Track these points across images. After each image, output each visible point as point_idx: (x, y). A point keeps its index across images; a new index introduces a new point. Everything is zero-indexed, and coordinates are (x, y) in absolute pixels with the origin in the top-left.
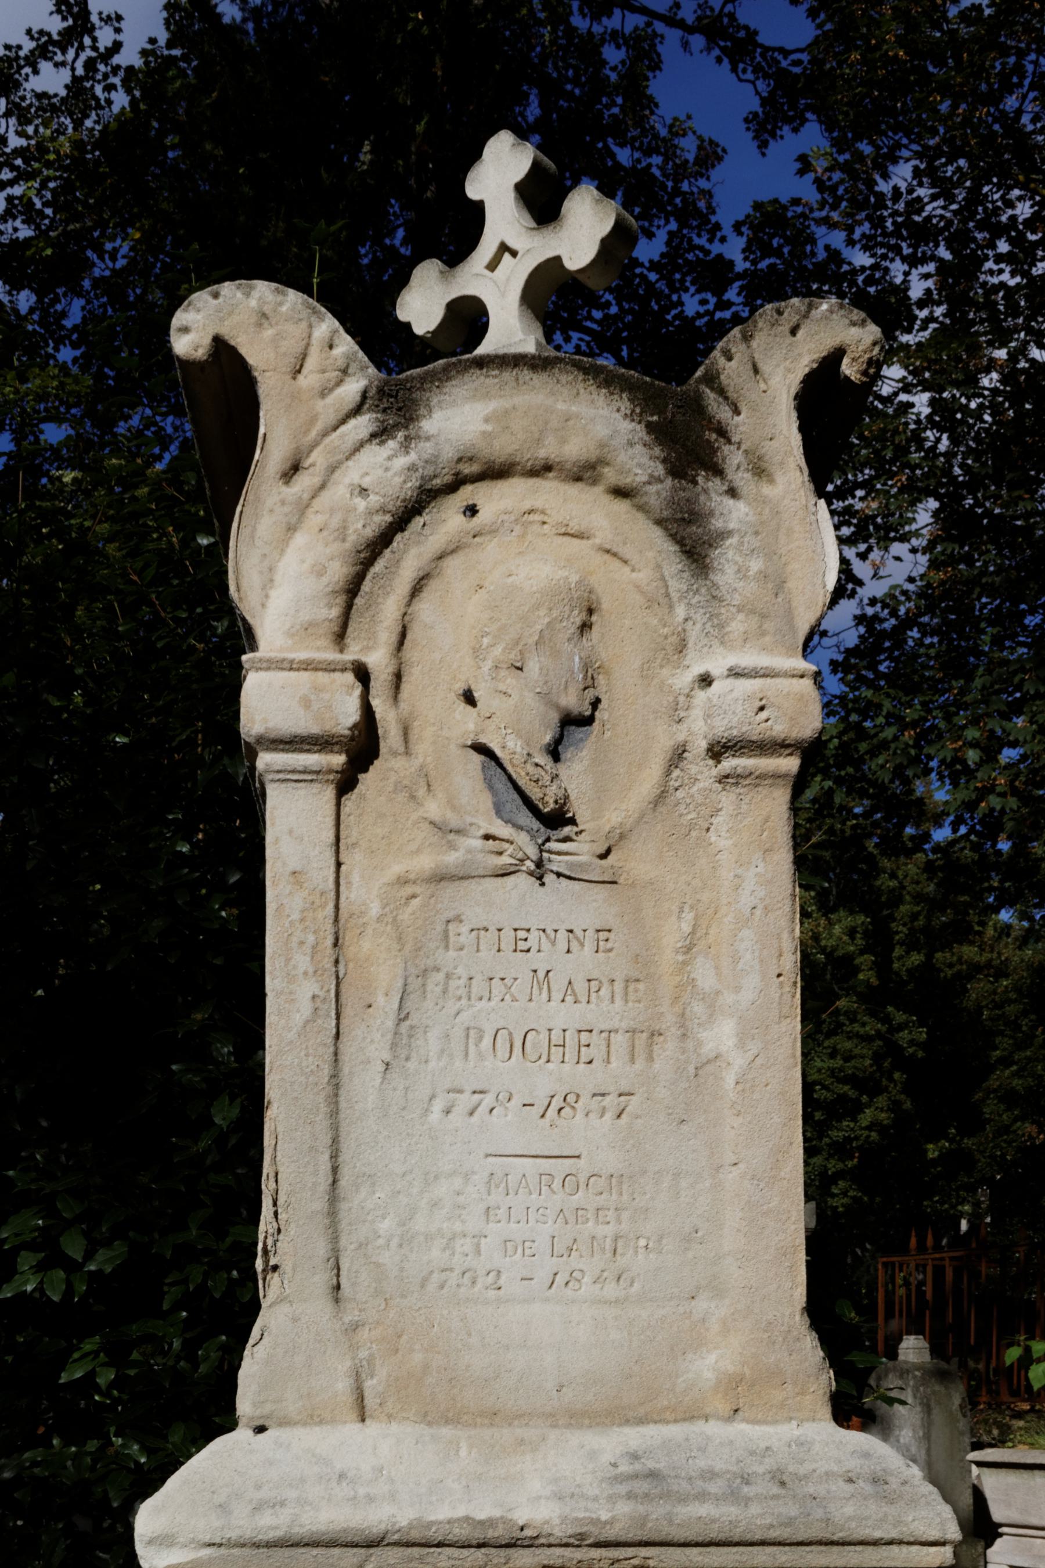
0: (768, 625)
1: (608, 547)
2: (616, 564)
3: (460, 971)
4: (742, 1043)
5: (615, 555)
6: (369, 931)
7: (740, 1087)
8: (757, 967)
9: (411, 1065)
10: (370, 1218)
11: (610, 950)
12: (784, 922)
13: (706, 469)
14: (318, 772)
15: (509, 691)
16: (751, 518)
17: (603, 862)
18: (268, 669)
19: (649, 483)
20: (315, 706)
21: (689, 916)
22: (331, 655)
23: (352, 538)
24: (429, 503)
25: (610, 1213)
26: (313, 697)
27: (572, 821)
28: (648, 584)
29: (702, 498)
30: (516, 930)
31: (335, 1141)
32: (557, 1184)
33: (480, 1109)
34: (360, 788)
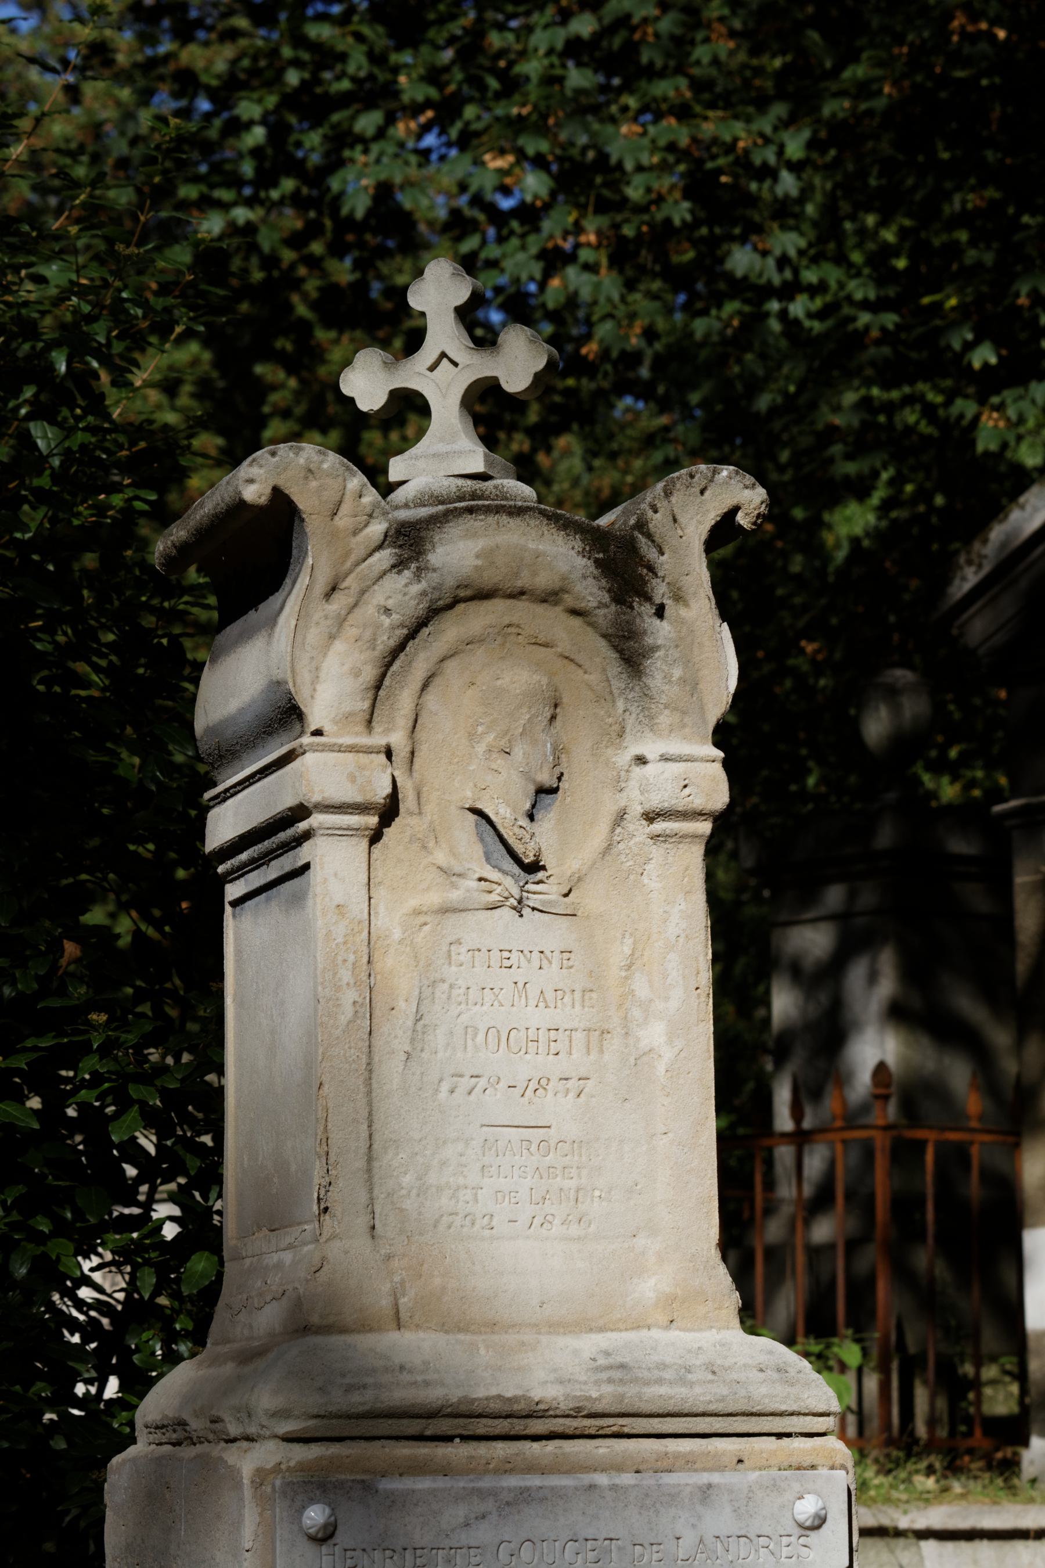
1: (567, 655)
2: (572, 667)
3: (460, 982)
4: (670, 1041)
5: (572, 660)
7: (669, 1074)
8: (681, 982)
10: (395, 1174)
11: (571, 967)
12: (700, 948)
13: (639, 596)
14: (357, 829)
15: (500, 770)
16: (673, 635)
17: (566, 899)
18: (323, 751)
19: (599, 608)
20: (359, 781)
21: (629, 941)
23: (380, 647)
25: (573, 1170)
26: (357, 774)
27: (544, 868)
31: (370, 1114)
32: (534, 1148)
33: (476, 1089)
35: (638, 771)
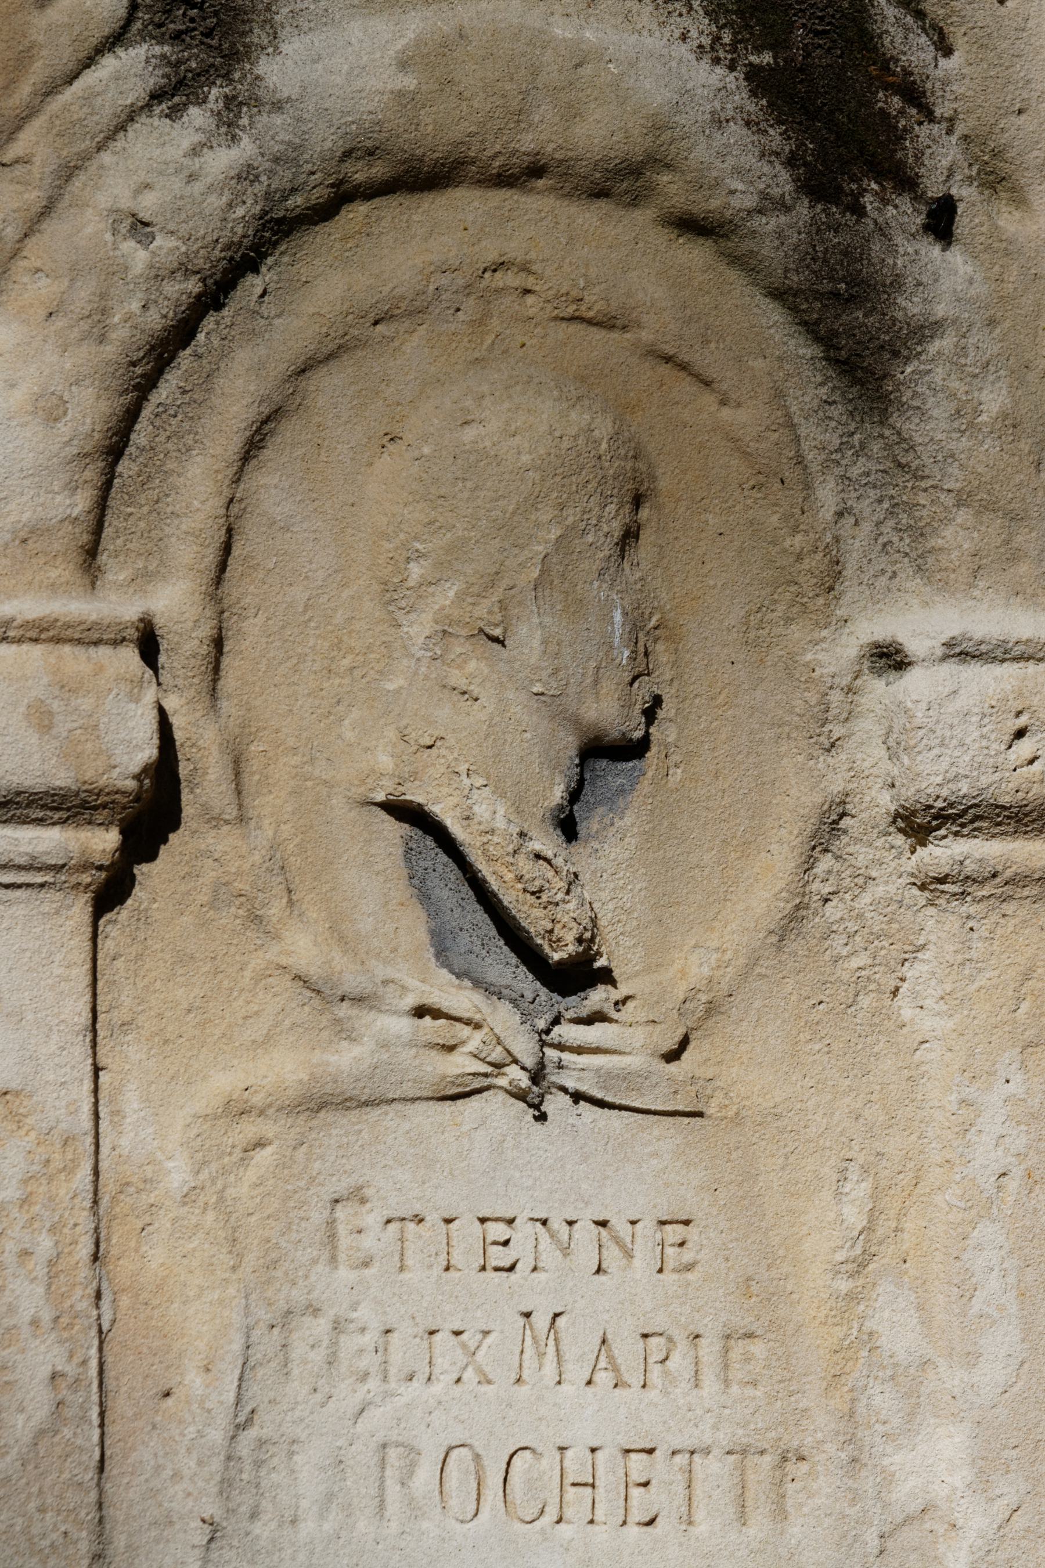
0: (1025, 538)
2: (686, 386)
3: (364, 1314)
4: (982, 1483)
5: (683, 367)
6: (163, 1222)
8: (1014, 1309)
9: (263, 1529)
11: (689, 1267)
14: (58, 868)
17: (673, 1067)
20: (61, 728)
21: (859, 1189)
23: (120, 334)
24: (275, 244)
26: (56, 705)
27: (606, 977)
29: (876, 247)
30: (483, 1220)
34: (139, 894)
35: (879, 689)
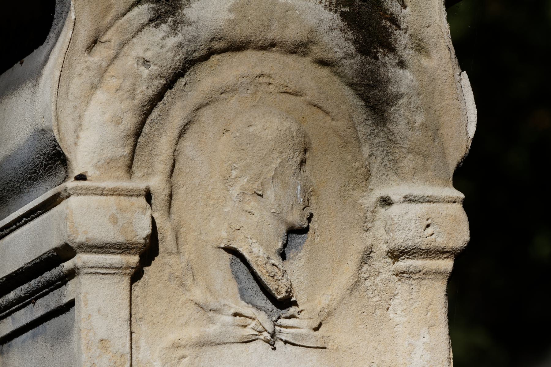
2: (321, 114)
5: (320, 108)
13: (383, 47)
14: (119, 268)
15: (253, 211)
16: (415, 83)
17: (316, 333)
18: (86, 194)
19: (345, 58)
20: (120, 223)
22: (126, 184)
23: (139, 97)
24: (189, 68)
27: (295, 304)
28: (344, 131)
35: (383, 212)
